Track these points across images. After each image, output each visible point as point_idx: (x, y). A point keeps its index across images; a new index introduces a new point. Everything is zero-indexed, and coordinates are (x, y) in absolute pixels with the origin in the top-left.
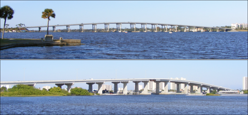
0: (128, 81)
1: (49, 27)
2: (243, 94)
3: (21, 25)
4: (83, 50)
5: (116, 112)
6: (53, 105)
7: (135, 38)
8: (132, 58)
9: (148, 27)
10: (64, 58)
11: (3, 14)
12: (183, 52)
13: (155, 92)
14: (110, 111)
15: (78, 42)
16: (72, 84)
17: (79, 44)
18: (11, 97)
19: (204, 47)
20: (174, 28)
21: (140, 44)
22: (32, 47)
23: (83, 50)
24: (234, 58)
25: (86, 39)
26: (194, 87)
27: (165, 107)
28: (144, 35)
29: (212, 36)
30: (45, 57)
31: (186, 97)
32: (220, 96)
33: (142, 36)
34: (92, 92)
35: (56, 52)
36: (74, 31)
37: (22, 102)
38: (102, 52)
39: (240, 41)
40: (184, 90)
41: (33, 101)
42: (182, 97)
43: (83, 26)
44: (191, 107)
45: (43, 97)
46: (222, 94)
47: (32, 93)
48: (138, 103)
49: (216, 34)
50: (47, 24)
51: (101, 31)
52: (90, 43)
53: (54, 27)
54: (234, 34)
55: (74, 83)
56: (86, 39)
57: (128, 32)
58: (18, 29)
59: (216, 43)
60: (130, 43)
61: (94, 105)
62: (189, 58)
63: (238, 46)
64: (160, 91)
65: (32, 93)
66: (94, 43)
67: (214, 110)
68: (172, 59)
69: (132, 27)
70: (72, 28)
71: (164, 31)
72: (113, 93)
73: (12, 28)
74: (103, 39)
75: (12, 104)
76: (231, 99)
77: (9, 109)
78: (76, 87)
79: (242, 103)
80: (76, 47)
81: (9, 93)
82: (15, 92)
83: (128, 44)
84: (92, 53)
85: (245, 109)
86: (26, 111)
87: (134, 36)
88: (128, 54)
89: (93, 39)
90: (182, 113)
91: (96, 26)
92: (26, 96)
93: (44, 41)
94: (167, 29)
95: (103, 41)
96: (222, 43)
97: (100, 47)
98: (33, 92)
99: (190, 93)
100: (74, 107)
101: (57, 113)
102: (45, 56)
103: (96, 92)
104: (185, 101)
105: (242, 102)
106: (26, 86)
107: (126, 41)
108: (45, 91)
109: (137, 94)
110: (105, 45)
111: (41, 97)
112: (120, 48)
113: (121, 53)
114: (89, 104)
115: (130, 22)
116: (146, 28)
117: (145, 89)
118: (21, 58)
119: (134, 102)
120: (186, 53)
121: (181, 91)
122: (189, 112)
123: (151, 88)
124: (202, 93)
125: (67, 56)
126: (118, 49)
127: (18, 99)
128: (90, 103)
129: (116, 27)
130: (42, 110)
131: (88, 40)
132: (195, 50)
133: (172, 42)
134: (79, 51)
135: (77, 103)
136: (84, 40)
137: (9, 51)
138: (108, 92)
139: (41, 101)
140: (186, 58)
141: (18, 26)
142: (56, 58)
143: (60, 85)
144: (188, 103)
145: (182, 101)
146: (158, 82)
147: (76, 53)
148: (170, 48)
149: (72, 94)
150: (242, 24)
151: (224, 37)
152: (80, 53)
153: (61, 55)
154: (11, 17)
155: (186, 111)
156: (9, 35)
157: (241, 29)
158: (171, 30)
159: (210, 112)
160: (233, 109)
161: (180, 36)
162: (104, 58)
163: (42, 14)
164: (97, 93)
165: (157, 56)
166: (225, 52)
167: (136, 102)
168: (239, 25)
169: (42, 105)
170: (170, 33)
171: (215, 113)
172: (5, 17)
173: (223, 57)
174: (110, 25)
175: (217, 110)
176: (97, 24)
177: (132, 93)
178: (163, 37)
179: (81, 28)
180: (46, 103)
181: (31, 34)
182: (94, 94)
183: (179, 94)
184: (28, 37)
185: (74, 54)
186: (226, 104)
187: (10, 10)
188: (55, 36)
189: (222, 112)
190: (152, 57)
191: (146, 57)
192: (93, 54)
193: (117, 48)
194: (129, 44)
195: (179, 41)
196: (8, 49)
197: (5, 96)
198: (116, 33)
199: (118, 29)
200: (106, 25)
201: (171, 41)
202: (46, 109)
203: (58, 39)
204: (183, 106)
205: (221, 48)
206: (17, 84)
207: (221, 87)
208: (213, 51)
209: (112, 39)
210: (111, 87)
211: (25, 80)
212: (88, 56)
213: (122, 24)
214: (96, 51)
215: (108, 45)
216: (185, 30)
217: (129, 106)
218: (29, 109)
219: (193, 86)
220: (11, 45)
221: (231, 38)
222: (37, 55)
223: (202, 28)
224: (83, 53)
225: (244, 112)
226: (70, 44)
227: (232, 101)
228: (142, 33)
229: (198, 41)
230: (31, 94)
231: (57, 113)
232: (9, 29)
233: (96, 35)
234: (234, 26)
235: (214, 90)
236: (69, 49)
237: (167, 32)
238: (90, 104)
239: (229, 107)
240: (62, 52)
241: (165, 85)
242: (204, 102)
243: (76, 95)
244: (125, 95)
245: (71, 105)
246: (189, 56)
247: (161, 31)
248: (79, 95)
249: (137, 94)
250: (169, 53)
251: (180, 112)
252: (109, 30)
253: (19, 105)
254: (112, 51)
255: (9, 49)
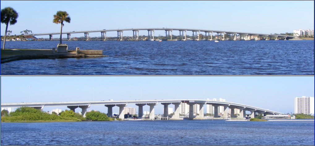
0: (155, 103)
1: (62, 34)
2: (295, 120)
3: (27, 32)
4: (106, 64)
5: (140, 142)
6: (65, 133)
7: (172, 48)
8: (167, 73)
9: (188, 35)
10: (81, 74)
11: (4, 18)
12: (233, 66)
13: (188, 116)
14: (134, 140)
15: (100, 53)
16: (88, 106)
17: (101, 56)
18: (14, 123)
19: (259, 59)
20: (220, 35)
21: (178, 56)
22: (40, 60)
23: (106, 63)
24: (296, 74)
25: (110, 49)
26: (235, 109)
27: (201, 135)
28: (183, 45)
29: (269, 46)
30: (58, 72)
31: (226, 123)
32: (267, 121)
33: (181, 45)
34: (112, 117)
35: (71, 65)
36: (94, 39)
37: (27, 129)
38: (130, 66)
39: (304, 52)
40: (223, 114)
41: (40, 128)
42: (221, 123)
43: (105, 34)
44: (231, 136)
45: (53, 123)
46: (270, 119)
47: (39, 118)
48: (167, 130)
49: (274, 42)
50: (60, 30)
51: (128, 40)
52: (115, 54)
53: (68, 34)
54: (297, 43)
55: (89, 105)
56: (110, 49)
57: (162, 40)
58: (24, 37)
59: (274, 55)
60: (165, 54)
61: (114, 132)
62: (239, 73)
63: (302, 58)
64: (194, 115)
65: (39, 117)
66: (119, 55)
67: (259, 139)
68: (218, 74)
69: (168, 34)
70: (91, 35)
71: (208, 39)
72: (137, 118)
73: (15, 35)
74: (131, 49)
75: (15, 132)
76: (281, 125)
77: (12, 139)
78: (92, 110)
79: (293, 131)
80: (96, 59)
81: (11, 118)
82: (19, 117)
83: (163, 55)
84: (117, 67)
85: (298, 138)
86: (32, 141)
87: (170, 45)
88: (162, 68)
89: (118, 50)
90: (220, 143)
91: (122, 32)
92: (31, 121)
93: (56, 52)
94: (213, 36)
95: (131, 52)
96: (281, 54)
97: (127, 60)
98: (41, 117)
99: (230, 118)
100: (89, 136)
101: (69, 143)
102: (57, 70)
103: (117, 116)
104: (224, 128)
105: (294, 129)
106: (31, 109)
107: (159, 52)
108: (55, 115)
109: (166, 119)
110: (134, 57)
111: (50, 123)
112: (152, 61)
113: (154, 67)
114: (108, 131)
115: (165, 28)
116: (185, 35)
117: (176, 113)
118: (27, 74)
119: (163, 129)
120: (236, 67)
121: (219, 116)
122: (229, 142)
123: (183, 111)
124: (246, 118)
125: (85, 70)
126: (150, 62)
127: (22, 126)
128: (110, 131)
129: (147, 35)
130: (51, 139)
131: (112, 50)
132: (247, 64)
133: (219, 54)
134: (100, 65)
135: (94, 130)
136: (107, 51)
137: (12, 65)
138: (131, 117)
139: (50, 128)
140: (236, 73)
141: (23, 33)
142: (71, 73)
143: (73, 108)
144: (229, 131)
145: (220, 128)
146: (192, 104)
147: (97, 67)
148: (216, 61)
149: (88, 119)
150: (307, 30)
151: (284, 46)
152: (101, 67)
153: (77, 70)
154: (14, 22)
155: (226, 141)
156: (12, 44)
157: (306, 36)
158: (216, 38)
159: (254, 142)
160: (283, 138)
161: (228, 46)
162: (132, 73)
163: (53, 18)
164: (118, 117)
165: (199, 71)
166: (286, 66)
167: (165, 129)
168: (304, 31)
169: (51, 133)
170: (216, 41)
171: (261, 143)
172: (6, 22)
173: (284, 72)
174: (140, 31)
175: (263, 140)
176: (124, 31)
177: (160, 117)
178: (207, 47)
179: (103, 35)
180: (56, 131)
181: (40, 43)
182: (114, 120)
183: (218, 119)
184: (36, 47)
185: (95, 69)
186: (274, 132)
187: (13, 13)
188: (70, 46)
189: (269, 141)
190: (193, 73)
191: (185, 73)
192: (118, 69)
193: (149, 61)
194: (164, 56)
195: (227, 53)
196: (11, 62)
197: (6, 122)
198: (148, 41)
199: (150, 37)
200: (135, 32)
201: (217, 52)
202: (56, 138)
203: (74, 50)
204: (222, 134)
205: (281, 61)
206: (21, 107)
207: (268, 110)
208: (271, 65)
209: (143, 49)
210: (135, 111)
211: (30, 101)
212: (113, 71)
213: (155, 31)
214: (123, 64)
215: (137, 57)
216: (235, 38)
217: (157, 135)
218: (35, 138)
219: (235, 109)
220: (15, 57)
221: (293, 49)
222: (47, 70)
223: (256, 36)
224: (106, 67)
225: (295, 141)
226: (89, 56)
227: (281, 128)
228: (181, 42)
229: (251, 53)
230: (38, 119)
231: (69, 143)
232: (11, 37)
233: (122, 44)
234: (297, 33)
235: (260, 114)
236: (87, 62)
237: (212, 40)
238: (110, 131)
239: (278, 136)
240: (79, 65)
241: (201, 108)
242: (247, 129)
243: (93, 121)
244: (151, 121)
245: (86, 133)
246: (239, 71)
247: (205, 39)
248: (96, 120)
249: (166, 119)
250: (214, 67)
251: (218, 142)
252: (139, 37)
253: (24, 133)
254: (142, 65)
255: (12, 62)
